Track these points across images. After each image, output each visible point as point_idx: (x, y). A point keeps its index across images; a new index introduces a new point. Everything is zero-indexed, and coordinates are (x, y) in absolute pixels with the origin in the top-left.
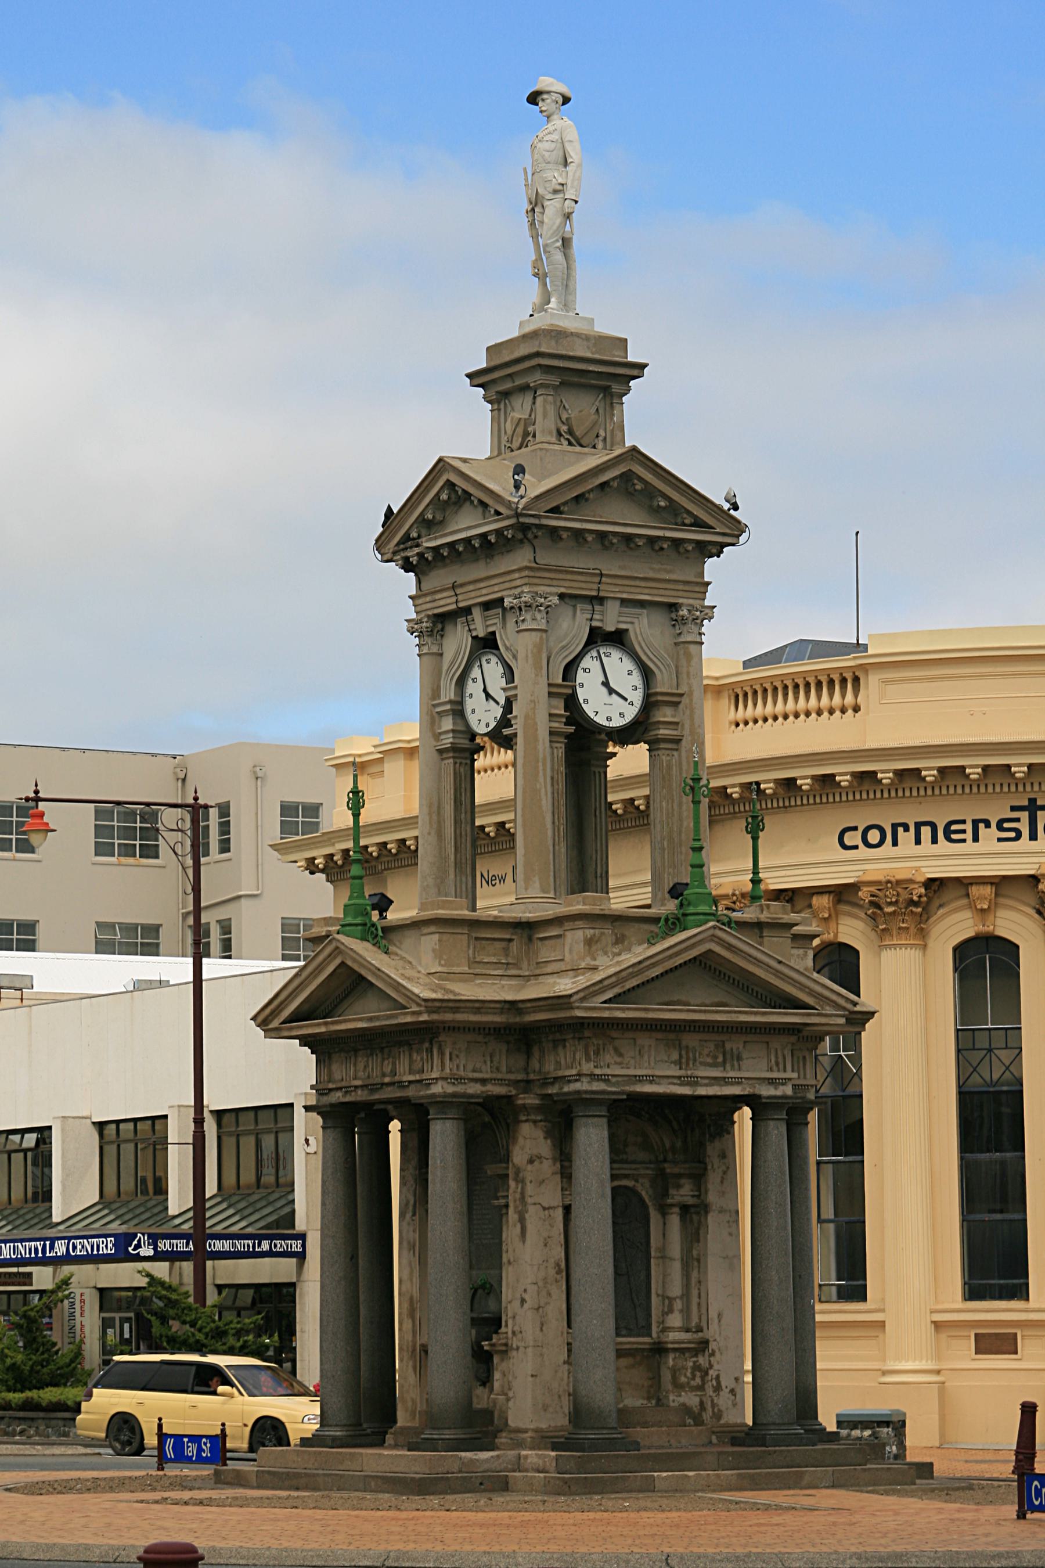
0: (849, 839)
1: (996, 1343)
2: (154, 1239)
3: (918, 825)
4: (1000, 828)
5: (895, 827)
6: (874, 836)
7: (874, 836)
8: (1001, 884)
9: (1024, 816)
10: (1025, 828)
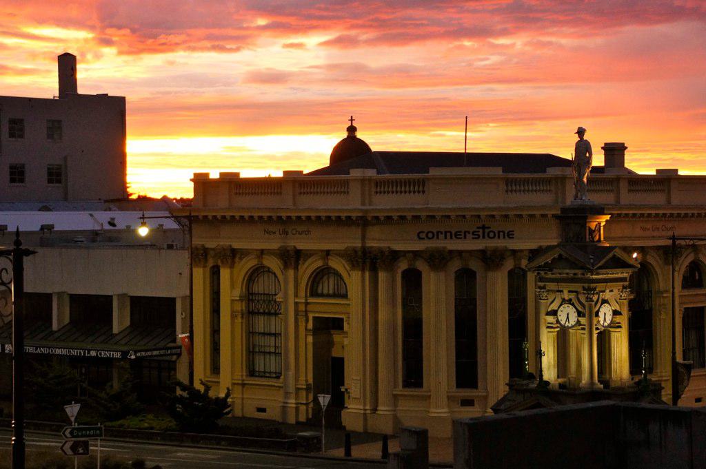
0: (423, 235)
1: (468, 402)
2: (135, 352)
3: (446, 232)
4: (473, 234)
5: (438, 232)
6: (430, 235)
7: (430, 235)
8: (471, 252)
9: (481, 230)
10: (481, 233)
